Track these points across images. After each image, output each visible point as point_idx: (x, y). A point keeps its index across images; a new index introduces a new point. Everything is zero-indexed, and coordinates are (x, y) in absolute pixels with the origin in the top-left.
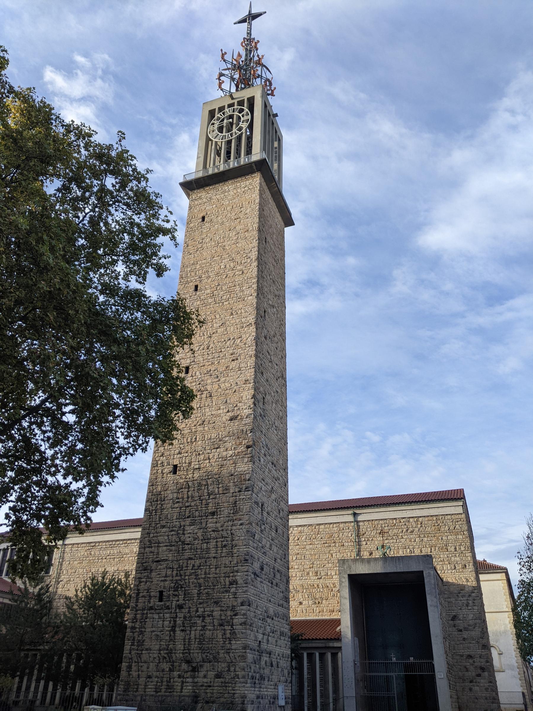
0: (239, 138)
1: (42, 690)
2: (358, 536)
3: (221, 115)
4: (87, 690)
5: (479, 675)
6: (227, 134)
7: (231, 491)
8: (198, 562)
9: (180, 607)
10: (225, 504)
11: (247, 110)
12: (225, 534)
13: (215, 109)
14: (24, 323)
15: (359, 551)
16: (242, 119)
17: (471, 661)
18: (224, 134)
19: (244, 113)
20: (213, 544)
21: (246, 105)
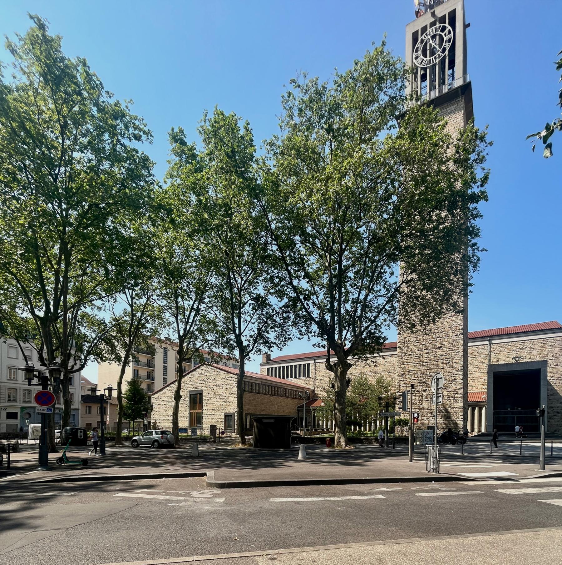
0: (443, 62)
1: (509, 493)
2: (490, 352)
3: (424, 37)
4: (188, 329)
5: (556, 415)
6: (431, 58)
7: (451, 335)
8: (432, 371)
9: (425, 391)
10: (447, 343)
11: (450, 28)
12: (447, 357)
13: (418, 30)
14: (444, 228)
15: (490, 359)
16: (445, 39)
17: (552, 409)
18: (428, 58)
19: (447, 30)
20: (441, 362)
21: (447, 21)
